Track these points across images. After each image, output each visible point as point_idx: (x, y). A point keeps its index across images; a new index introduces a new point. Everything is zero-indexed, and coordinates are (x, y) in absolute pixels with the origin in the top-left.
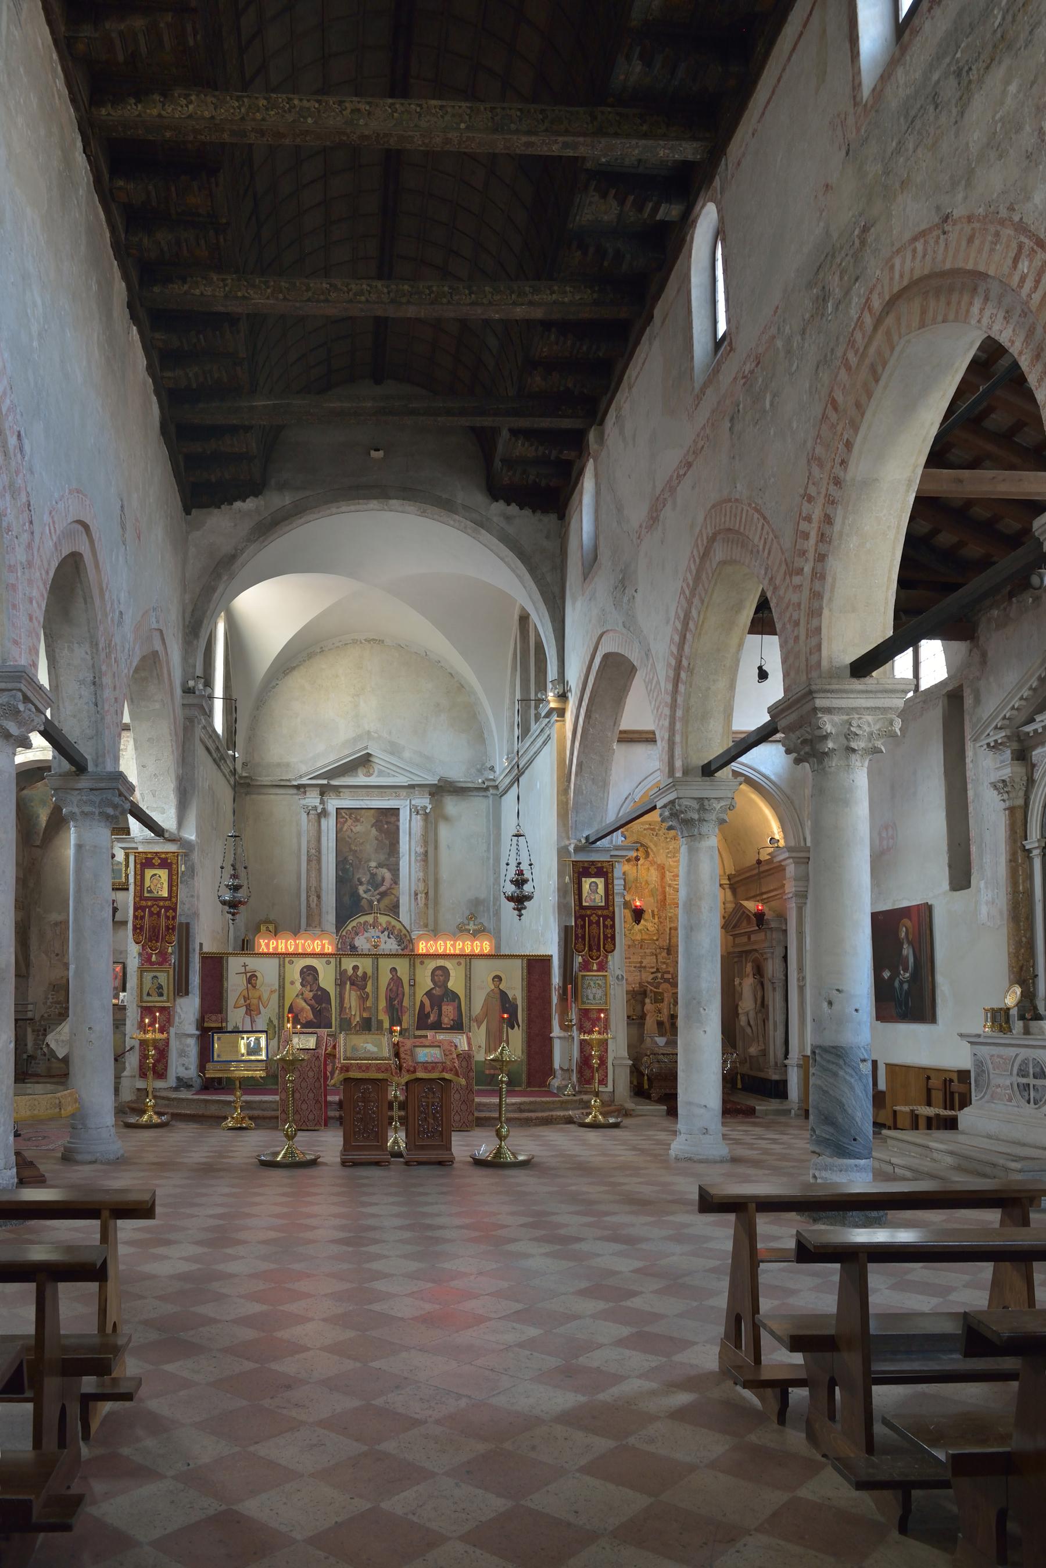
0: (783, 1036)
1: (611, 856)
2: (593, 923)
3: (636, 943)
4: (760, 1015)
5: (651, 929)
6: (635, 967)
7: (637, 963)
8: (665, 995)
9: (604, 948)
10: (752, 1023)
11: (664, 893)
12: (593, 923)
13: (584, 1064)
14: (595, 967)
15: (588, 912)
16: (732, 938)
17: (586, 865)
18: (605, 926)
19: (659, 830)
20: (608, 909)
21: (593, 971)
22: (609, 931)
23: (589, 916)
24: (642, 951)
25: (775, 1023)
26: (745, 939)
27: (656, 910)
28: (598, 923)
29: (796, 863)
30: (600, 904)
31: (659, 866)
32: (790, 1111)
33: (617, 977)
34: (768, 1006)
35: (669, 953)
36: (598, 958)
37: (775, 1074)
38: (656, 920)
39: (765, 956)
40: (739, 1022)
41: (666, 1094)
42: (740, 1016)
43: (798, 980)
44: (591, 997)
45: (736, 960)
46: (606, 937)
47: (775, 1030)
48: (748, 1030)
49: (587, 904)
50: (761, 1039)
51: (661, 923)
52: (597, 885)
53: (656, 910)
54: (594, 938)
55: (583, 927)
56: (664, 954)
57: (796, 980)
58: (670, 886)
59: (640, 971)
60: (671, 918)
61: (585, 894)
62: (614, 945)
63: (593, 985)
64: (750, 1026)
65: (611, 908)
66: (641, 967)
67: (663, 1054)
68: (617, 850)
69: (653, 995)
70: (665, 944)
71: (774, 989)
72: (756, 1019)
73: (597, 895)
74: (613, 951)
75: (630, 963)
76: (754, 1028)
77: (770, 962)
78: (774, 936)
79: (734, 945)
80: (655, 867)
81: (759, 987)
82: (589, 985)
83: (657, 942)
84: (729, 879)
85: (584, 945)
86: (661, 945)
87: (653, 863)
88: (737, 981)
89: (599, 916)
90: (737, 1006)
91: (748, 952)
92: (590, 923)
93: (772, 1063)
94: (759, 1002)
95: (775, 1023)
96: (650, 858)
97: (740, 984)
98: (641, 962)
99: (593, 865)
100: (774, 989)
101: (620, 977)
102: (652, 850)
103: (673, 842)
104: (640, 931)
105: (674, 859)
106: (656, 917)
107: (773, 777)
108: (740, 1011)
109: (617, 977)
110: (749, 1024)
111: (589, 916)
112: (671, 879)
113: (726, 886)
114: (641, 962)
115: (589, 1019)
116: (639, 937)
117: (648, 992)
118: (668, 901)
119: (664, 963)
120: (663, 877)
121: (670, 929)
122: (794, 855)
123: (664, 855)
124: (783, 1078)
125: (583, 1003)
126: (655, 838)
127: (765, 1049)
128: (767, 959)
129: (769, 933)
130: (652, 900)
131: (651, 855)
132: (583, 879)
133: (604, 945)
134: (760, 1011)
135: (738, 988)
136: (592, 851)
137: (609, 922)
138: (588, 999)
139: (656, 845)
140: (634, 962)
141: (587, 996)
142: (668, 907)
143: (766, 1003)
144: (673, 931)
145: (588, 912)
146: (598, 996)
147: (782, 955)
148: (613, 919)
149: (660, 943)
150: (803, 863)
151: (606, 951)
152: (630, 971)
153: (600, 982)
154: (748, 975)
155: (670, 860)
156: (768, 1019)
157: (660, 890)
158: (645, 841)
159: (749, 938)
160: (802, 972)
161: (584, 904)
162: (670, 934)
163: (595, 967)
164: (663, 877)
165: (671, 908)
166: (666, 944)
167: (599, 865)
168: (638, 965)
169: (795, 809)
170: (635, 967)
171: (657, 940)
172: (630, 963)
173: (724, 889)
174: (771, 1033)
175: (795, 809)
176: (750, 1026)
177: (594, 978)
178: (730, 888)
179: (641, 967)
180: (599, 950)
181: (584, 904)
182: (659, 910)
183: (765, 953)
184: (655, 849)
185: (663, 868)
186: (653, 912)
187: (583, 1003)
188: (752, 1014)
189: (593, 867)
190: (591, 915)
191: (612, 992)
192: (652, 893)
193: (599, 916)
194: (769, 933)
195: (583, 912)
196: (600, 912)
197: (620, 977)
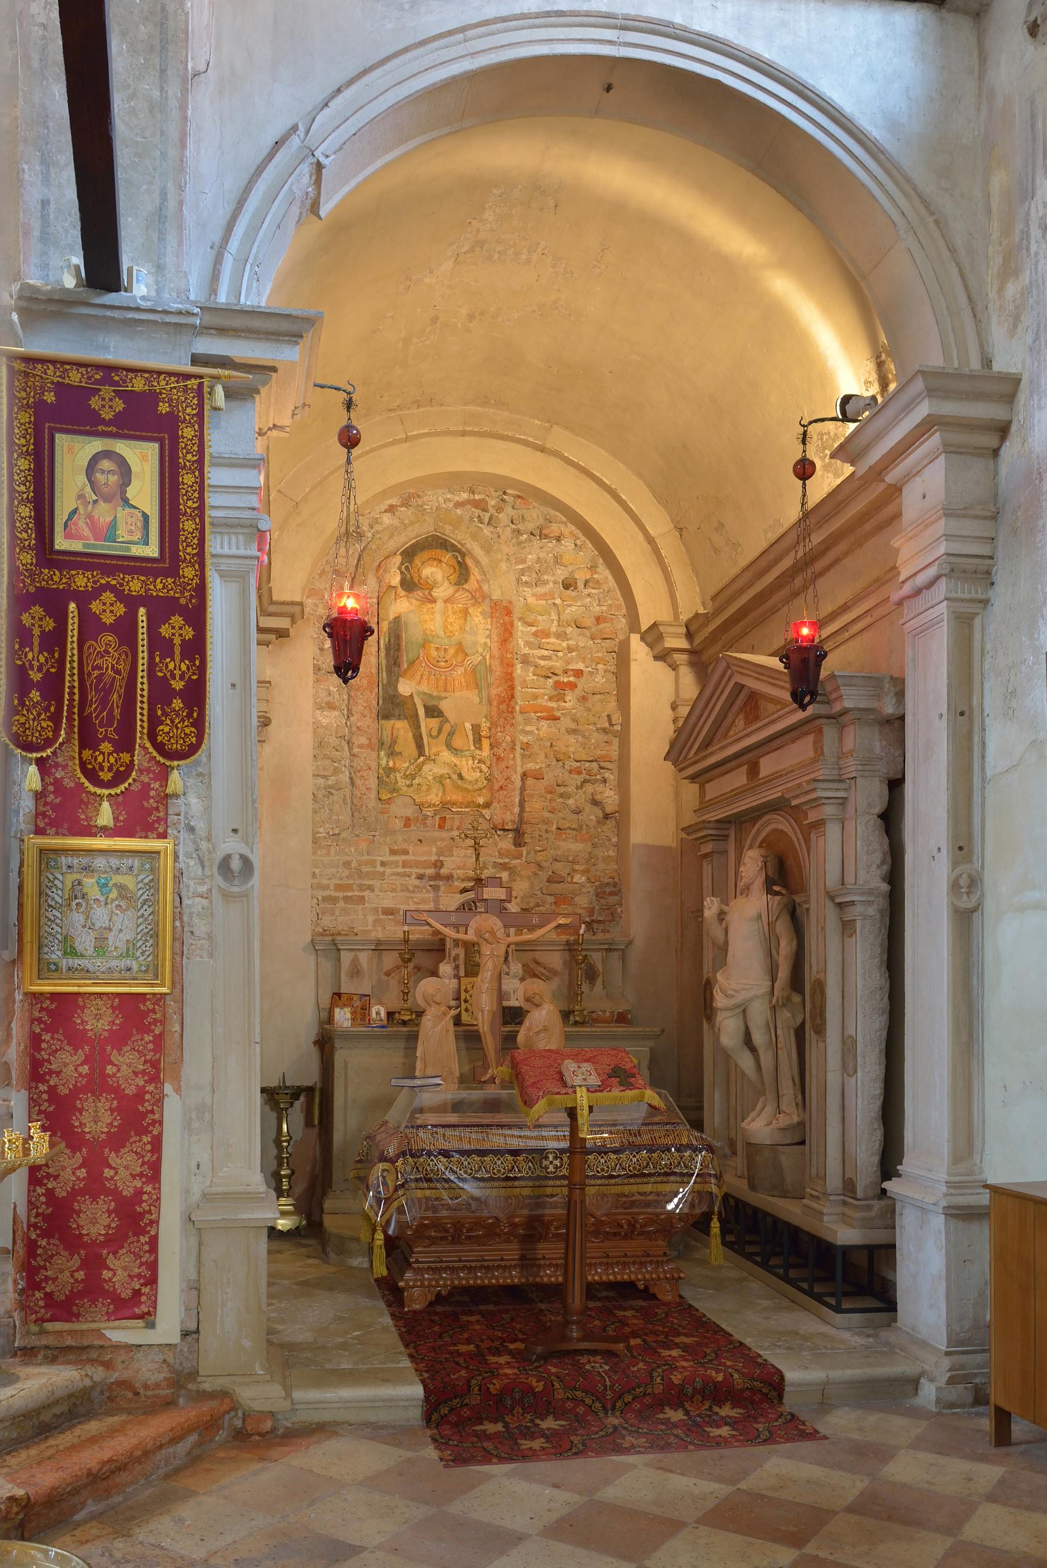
0: (877, 1089)
1: (196, 360)
2: (104, 628)
3: (429, 812)
4: (785, 1015)
5: (471, 775)
6: (420, 877)
7: (425, 865)
8: (486, 950)
9: (152, 736)
10: (759, 1038)
11: (509, 678)
12: (113, 628)
13: (46, 1234)
14: (105, 815)
15: (81, 581)
16: (694, 788)
17: (75, 377)
18: (159, 645)
19: (499, 510)
20: (173, 572)
21: (89, 831)
22: (176, 667)
23: (84, 599)
24: (444, 834)
25: (849, 1045)
26: (738, 779)
27: (485, 725)
28: (125, 630)
29: (950, 449)
30: (137, 551)
31: (495, 605)
32: (913, 1383)
33: (225, 865)
34: (820, 987)
35: (518, 843)
36: (119, 777)
37: (845, 1220)
38: (486, 752)
39: (812, 816)
40: (717, 1037)
41: (466, 1290)
42: (720, 1017)
43: (955, 886)
44: (85, 942)
45: (707, 848)
46: (160, 692)
47: (848, 1067)
48: (745, 1061)
49: (76, 546)
50: (788, 1090)
51: (499, 759)
52: (125, 472)
53: (485, 725)
54: (108, 691)
55: (55, 640)
56: (506, 843)
57: (944, 887)
58: (525, 661)
59: (436, 888)
60: (526, 747)
61: (65, 502)
62: (199, 725)
63: (94, 893)
64: (753, 1049)
65: (188, 572)
66: (437, 877)
67: (446, 1154)
68: (222, 331)
69: (461, 952)
70: (508, 817)
71: (847, 927)
72: (772, 1027)
73: (122, 513)
74: (193, 749)
75: (405, 864)
76: (766, 1059)
77: (833, 831)
78: (849, 743)
79: (704, 806)
80: (486, 607)
81: (783, 927)
82: (77, 893)
83: (486, 812)
84: (689, 636)
85: (56, 718)
86: (497, 820)
87: (478, 597)
88: (711, 907)
89: (132, 603)
90: (708, 987)
91: (741, 822)
92: (90, 627)
93: (834, 1181)
94: (784, 973)
95: (849, 1045)
96: (472, 584)
97: (721, 916)
98: (438, 864)
99: (107, 381)
100: (847, 927)
101: (236, 864)
102: (477, 562)
103: (536, 542)
104: (440, 779)
105: (541, 590)
106: (486, 743)
107: (876, 132)
108: (720, 1000)
109: (225, 865)
110: (748, 1041)
111: (84, 599)
112: (528, 643)
113: (681, 658)
114: (438, 864)
115: (76, 1039)
116: (434, 797)
117: (449, 944)
118: (520, 702)
119: (505, 867)
120: (507, 634)
121: (524, 775)
122: (950, 408)
123: (512, 578)
124: (878, 1237)
125: (46, 969)
126: (487, 531)
127: (801, 1124)
128: (820, 824)
129: (829, 733)
130: (473, 696)
131: (475, 574)
132: (62, 440)
133: (154, 722)
134: (787, 1002)
135: (715, 931)
136: (106, 324)
137: (176, 629)
138: (71, 951)
139: (488, 550)
140: (417, 864)
141: (67, 939)
142: (519, 718)
143: (810, 976)
144: (530, 782)
145: (81, 581)
146: (117, 940)
147: (878, 809)
148: (197, 617)
149: (495, 813)
150: (979, 452)
151: (159, 748)
152: (405, 889)
153: (128, 881)
154: (748, 888)
155: (528, 592)
156: (820, 1030)
157: (498, 670)
158: (459, 536)
159: (754, 770)
160: (969, 859)
161: (61, 543)
162: (523, 789)
163: (105, 815)
164: (507, 634)
165: (527, 722)
166: (510, 818)
167: (138, 385)
168: (431, 871)
169: (952, 250)
170: (420, 877)
171: (487, 805)
172: (405, 864)
173: (674, 667)
174: (833, 1078)
175: (952, 250)
176: (753, 1049)
177: (100, 862)
178: (692, 664)
179: (438, 878)
180: (125, 743)
181: (61, 543)
182: (493, 725)
183: (817, 804)
184: (484, 560)
185: (509, 612)
186: (476, 729)
187: (46, 969)
188: (759, 1013)
189: (107, 391)
190: (96, 593)
191: (201, 927)
192: (475, 680)
193: (132, 603)
194: (829, 733)
195: (56, 579)
196: (135, 586)
197: (236, 864)
